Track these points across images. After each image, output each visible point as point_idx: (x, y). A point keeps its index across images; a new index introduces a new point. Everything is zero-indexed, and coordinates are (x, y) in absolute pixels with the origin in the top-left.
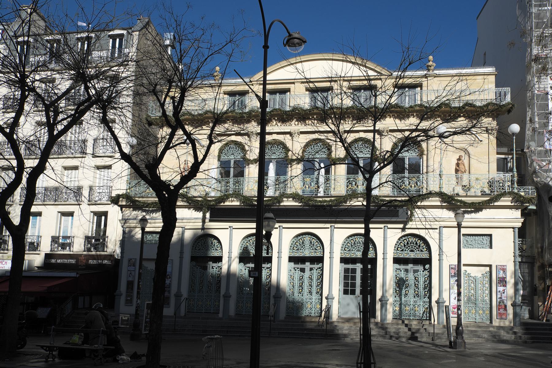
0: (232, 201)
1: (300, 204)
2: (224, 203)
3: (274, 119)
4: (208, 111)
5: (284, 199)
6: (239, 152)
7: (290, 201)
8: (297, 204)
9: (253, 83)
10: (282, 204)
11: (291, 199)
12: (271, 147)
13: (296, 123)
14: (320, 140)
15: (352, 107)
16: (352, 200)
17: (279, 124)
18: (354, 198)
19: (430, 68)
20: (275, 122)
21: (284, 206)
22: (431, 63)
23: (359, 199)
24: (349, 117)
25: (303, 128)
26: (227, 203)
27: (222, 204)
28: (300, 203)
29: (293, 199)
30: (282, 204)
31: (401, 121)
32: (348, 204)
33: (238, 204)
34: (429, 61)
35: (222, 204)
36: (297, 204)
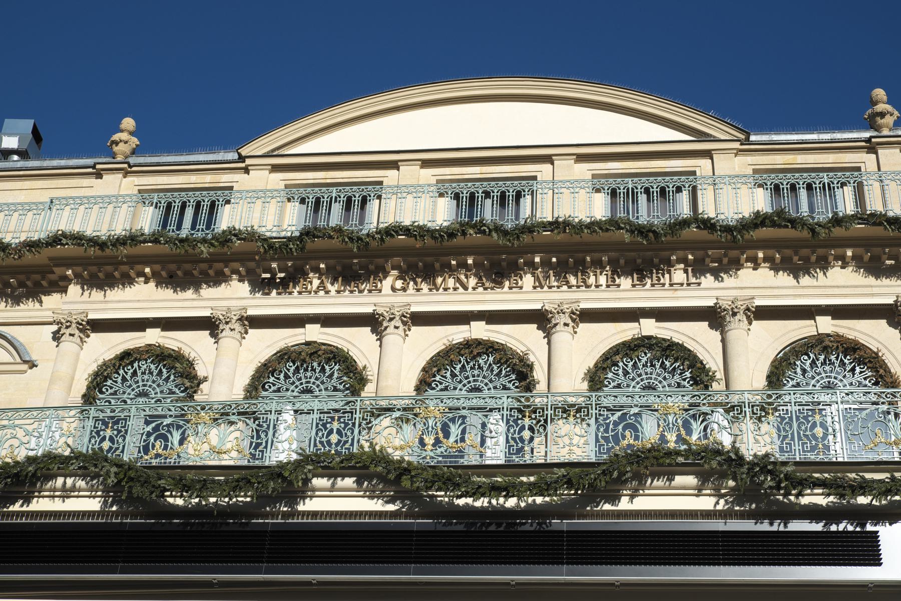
0: (66, 493)
1: (391, 507)
2: (27, 500)
3: (316, 270)
4: (64, 235)
5: (317, 482)
6: (171, 385)
7: (345, 493)
8: (376, 505)
9: (248, 161)
10: (309, 505)
11: (349, 482)
12: (297, 370)
13: (399, 284)
14: (490, 347)
15: (613, 223)
16: (642, 484)
17: (333, 289)
18: (655, 475)
19: (880, 121)
20: (316, 282)
21: (315, 514)
22: (880, 107)
23: (679, 480)
24: (598, 265)
25: (425, 299)
26: (40, 504)
27: (16, 507)
28: (391, 501)
29: (359, 482)
30: (309, 505)
31: (796, 277)
32: (624, 504)
33: (94, 505)
34: (875, 103)
35: (16, 507)
36: (376, 505)
